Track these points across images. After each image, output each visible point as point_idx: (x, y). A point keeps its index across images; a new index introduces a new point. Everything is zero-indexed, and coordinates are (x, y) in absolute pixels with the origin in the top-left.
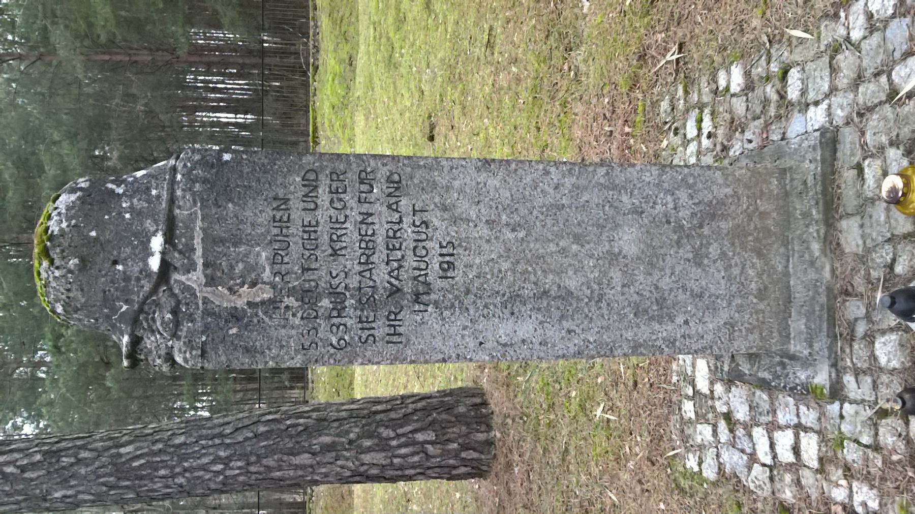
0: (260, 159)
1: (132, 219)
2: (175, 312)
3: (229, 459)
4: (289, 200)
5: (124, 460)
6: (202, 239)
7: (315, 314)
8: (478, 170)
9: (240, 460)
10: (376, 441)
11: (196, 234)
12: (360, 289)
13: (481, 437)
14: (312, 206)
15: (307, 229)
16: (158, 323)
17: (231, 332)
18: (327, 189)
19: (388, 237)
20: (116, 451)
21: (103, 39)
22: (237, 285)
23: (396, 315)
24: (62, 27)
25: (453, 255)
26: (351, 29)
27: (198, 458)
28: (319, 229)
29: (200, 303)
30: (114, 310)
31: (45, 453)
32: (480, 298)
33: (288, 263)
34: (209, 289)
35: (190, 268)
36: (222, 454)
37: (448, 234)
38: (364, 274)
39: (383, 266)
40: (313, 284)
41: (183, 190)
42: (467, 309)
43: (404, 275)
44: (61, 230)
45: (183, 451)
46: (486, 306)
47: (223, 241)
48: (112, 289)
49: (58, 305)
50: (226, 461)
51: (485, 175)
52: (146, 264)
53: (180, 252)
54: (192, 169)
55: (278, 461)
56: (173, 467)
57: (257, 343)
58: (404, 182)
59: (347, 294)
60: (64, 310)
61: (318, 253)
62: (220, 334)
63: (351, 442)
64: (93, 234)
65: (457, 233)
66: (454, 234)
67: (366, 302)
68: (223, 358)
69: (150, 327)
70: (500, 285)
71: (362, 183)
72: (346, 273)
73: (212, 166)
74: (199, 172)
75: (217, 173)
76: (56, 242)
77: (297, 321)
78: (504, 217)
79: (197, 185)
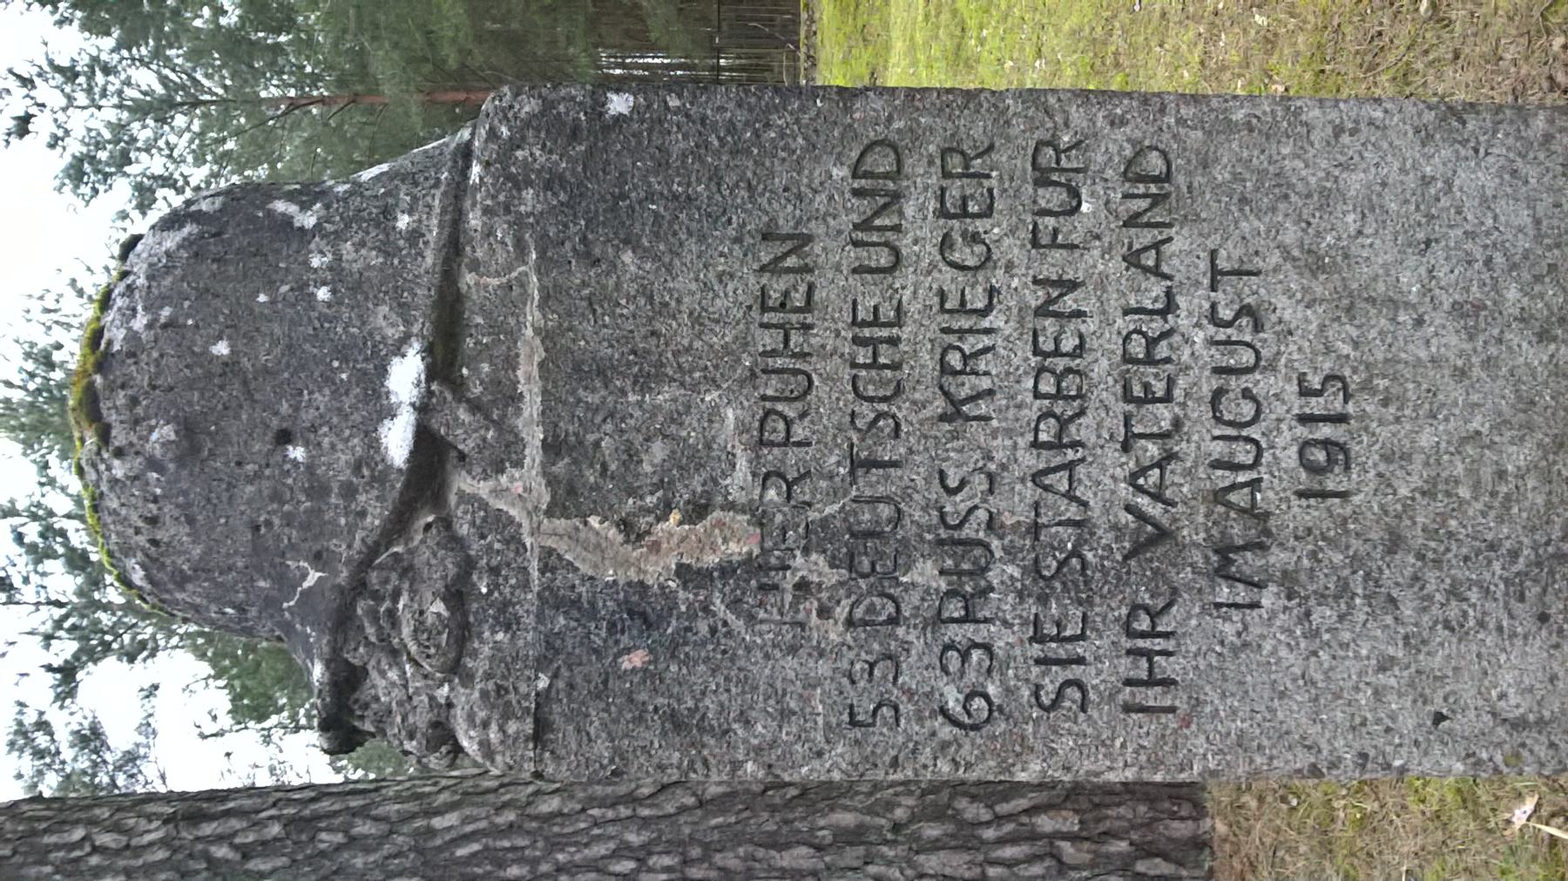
0: (721, 109)
1: (335, 302)
2: (457, 595)
3: (647, 849)
4: (809, 239)
5: (438, 842)
6: (541, 365)
7: (890, 608)
8: (1425, 136)
9: (667, 853)
10: (950, 828)
11: (523, 350)
12: (1035, 529)
13: (1181, 829)
14: (884, 259)
15: (867, 332)
16: (406, 631)
17: (626, 663)
18: (933, 205)
19: (1128, 359)
20: (424, 823)
21: (453, 63)
22: (649, 511)
23: (1154, 615)
24: (387, 44)
25: (1341, 419)
26: (875, 20)
27: (586, 845)
28: (905, 333)
29: (534, 568)
30: (286, 583)
31: (289, 822)
32: (1437, 563)
33: (805, 443)
34: (561, 524)
35: (505, 456)
36: (633, 838)
37: (1328, 350)
38: (1048, 480)
39: (1112, 454)
40: (885, 511)
41: (487, 211)
42: (1392, 601)
43: (1180, 485)
44: (132, 336)
45: (556, 829)
46: (1454, 592)
47: (603, 372)
48: (276, 521)
49: (131, 563)
50: (642, 854)
51: (1446, 152)
52: (374, 444)
53: (475, 407)
54: (515, 144)
55: (745, 859)
56: (534, 862)
57: (709, 702)
58: (1181, 179)
59: (995, 544)
60: (149, 577)
61: (902, 410)
62: (595, 668)
63: (897, 827)
64: (222, 349)
65: (1356, 345)
66: (1346, 349)
67: (1058, 574)
68: (602, 748)
69: (384, 639)
70: (1500, 520)
71: (1043, 181)
72: (991, 477)
73: (575, 134)
74: (532, 154)
75: (590, 152)
76: (117, 373)
77: (835, 633)
78: (1512, 294)
79: (529, 194)
